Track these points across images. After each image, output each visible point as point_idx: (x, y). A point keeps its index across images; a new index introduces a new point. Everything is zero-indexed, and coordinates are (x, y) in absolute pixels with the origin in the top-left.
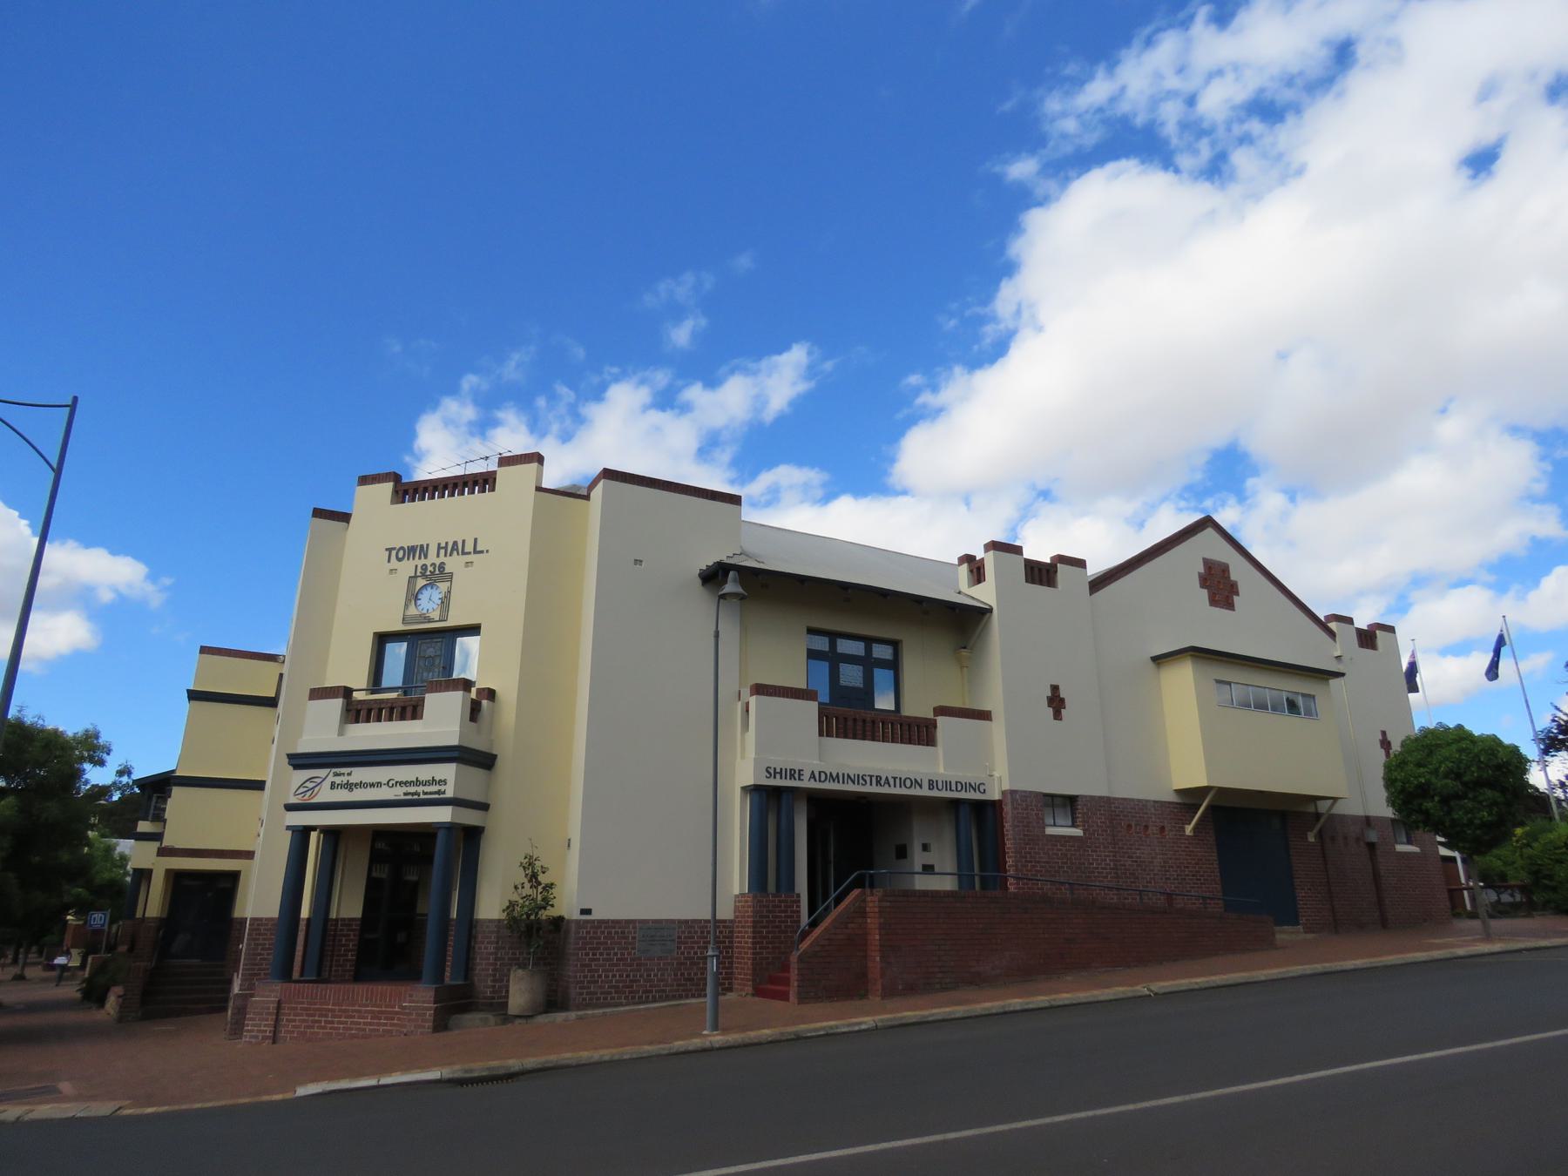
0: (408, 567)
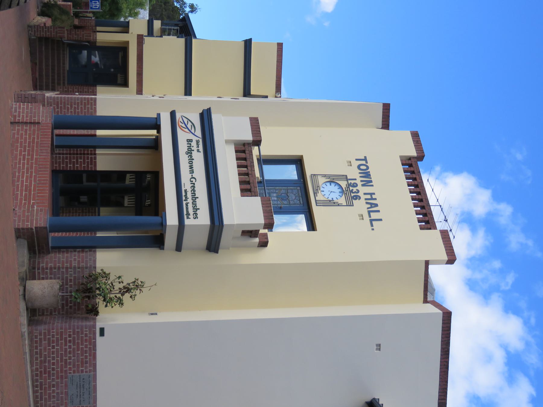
0: (354, 173)
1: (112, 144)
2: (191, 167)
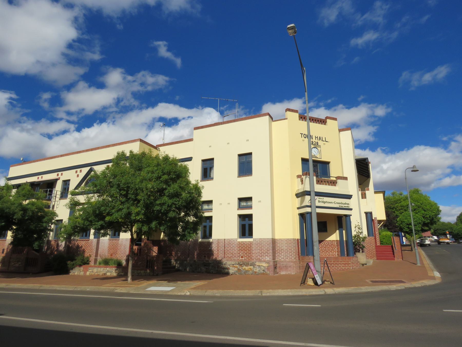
2: (330, 203)
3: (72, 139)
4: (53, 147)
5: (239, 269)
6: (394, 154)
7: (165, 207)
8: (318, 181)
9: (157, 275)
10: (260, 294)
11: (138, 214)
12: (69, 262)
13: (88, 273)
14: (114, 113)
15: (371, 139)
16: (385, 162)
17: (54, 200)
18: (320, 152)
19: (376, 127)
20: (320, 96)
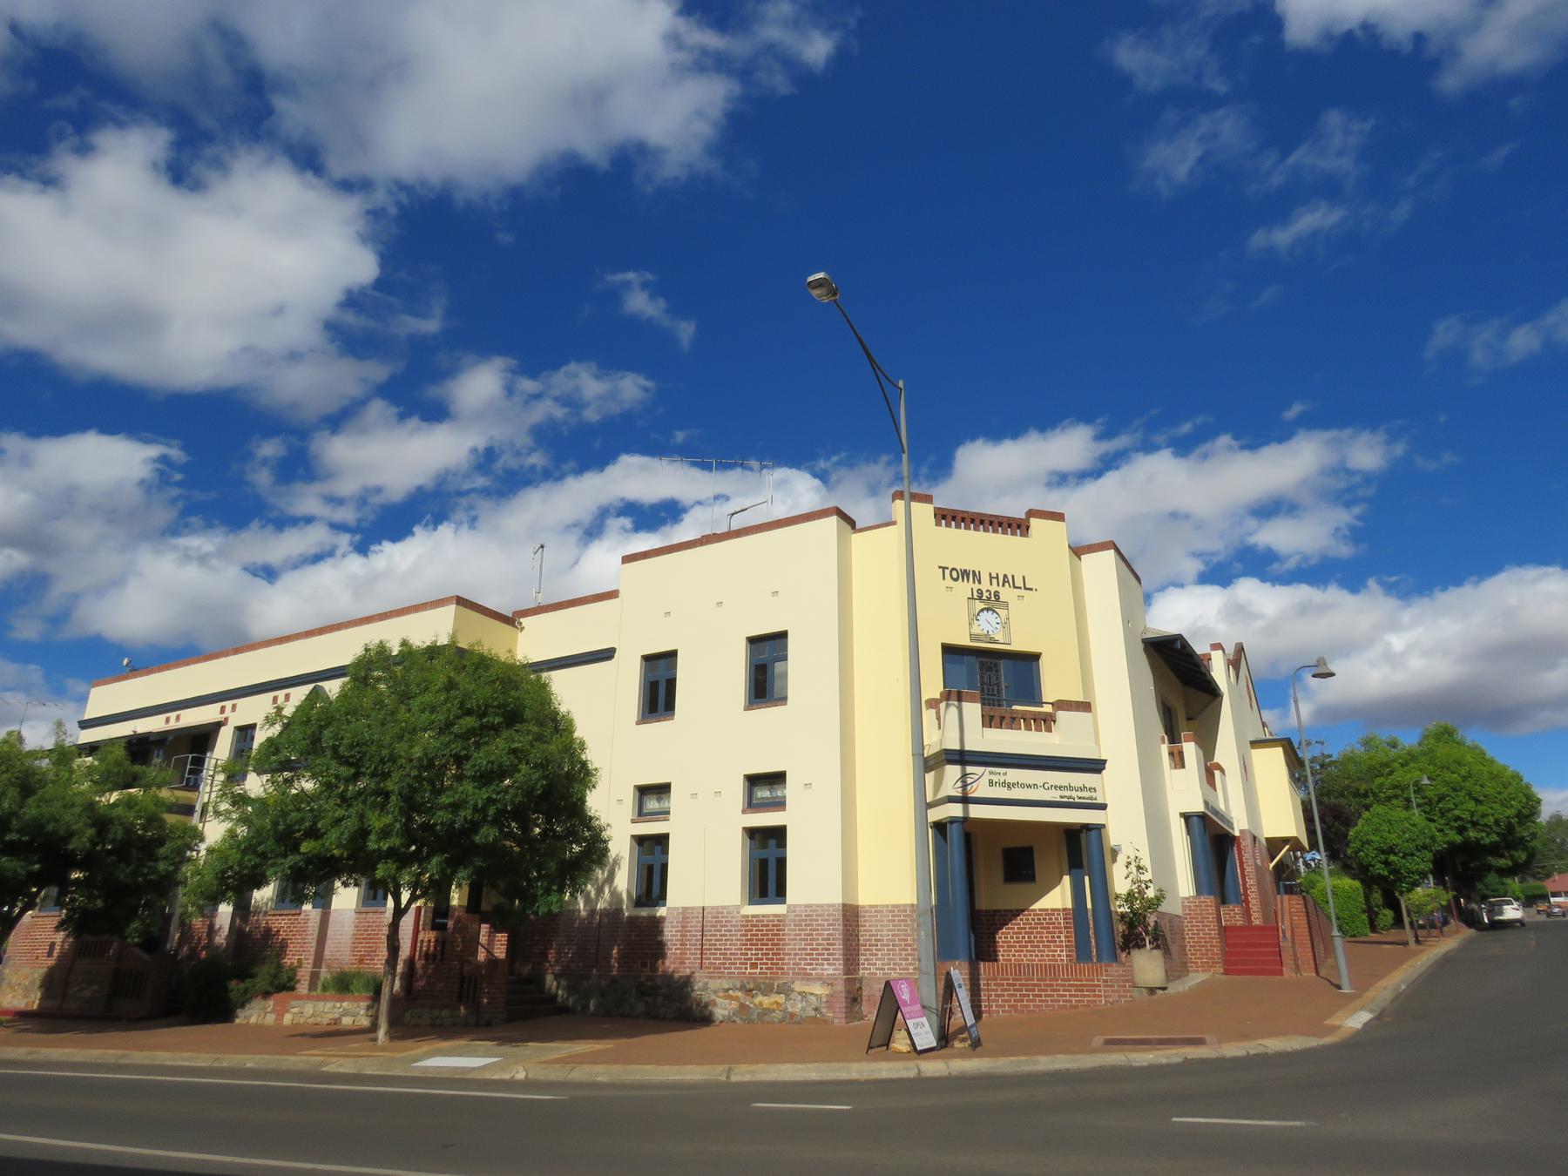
0: (965, 588)
1: (351, 631)
3: (340, 581)
4: (278, 606)
5: (743, 1006)
6: (1431, 595)
7: (466, 813)
8: (992, 718)
9: (489, 1024)
10: (723, 1078)
11: (385, 833)
12: (233, 984)
13: (287, 1019)
14: (473, 495)
15: (1344, 551)
16: (1395, 627)
17: (208, 789)
18: (1006, 624)
19: (1357, 510)
20: (1155, 412)
